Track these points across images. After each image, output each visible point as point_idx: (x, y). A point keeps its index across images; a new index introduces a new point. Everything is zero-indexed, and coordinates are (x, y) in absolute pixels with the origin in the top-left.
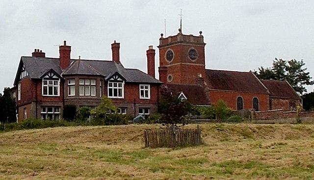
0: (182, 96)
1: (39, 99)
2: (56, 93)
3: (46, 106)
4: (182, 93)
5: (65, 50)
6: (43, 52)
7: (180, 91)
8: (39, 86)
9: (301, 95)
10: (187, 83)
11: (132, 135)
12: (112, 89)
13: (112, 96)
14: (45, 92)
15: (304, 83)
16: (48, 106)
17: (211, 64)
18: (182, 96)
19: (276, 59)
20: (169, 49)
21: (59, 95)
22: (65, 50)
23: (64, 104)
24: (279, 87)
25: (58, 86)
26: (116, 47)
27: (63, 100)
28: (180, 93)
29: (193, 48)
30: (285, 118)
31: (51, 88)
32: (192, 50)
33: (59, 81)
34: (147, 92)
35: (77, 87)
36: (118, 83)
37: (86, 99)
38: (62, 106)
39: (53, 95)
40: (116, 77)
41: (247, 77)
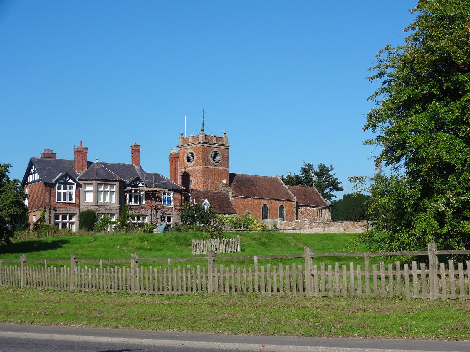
0: (206, 203)
1: (53, 205)
2: (71, 199)
3: (68, 214)
4: (206, 200)
5: (81, 152)
6: (53, 152)
7: (204, 198)
8: (52, 190)
9: (329, 202)
10: (209, 189)
11: (276, 251)
12: (60, 193)
13: (61, 200)
14: (59, 199)
15: (333, 190)
16: (62, 214)
17: (236, 167)
18: (206, 203)
19: (304, 162)
20: (190, 150)
21: (74, 201)
22: (81, 152)
23: (80, 211)
24: (306, 194)
25: (74, 191)
26: (136, 150)
27: (79, 207)
28: (203, 201)
29: (216, 150)
30: (312, 228)
31: (65, 194)
32: (215, 152)
33: (75, 186)
34: (70, 194)
35: (97, 193)
36: (68, 186)
37: (105, 206)
38: (78, 213)
39: (62, 201)
40: (136, 183)
41: (272, 181)
